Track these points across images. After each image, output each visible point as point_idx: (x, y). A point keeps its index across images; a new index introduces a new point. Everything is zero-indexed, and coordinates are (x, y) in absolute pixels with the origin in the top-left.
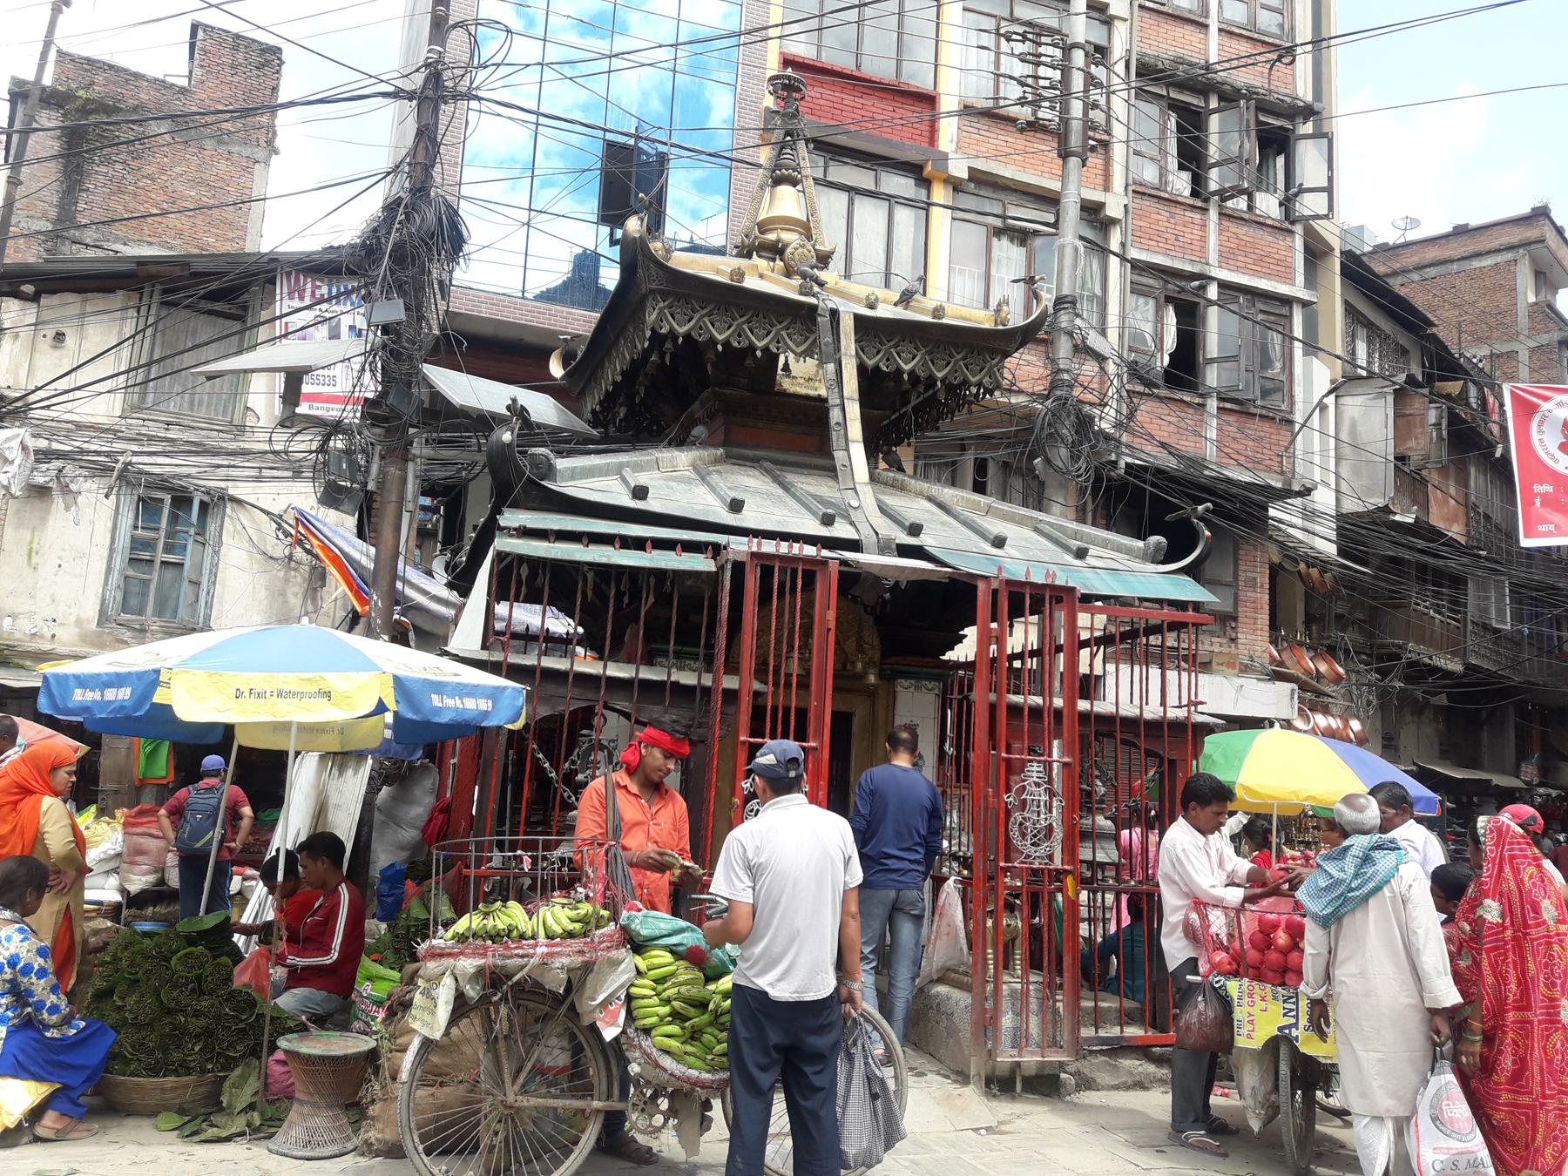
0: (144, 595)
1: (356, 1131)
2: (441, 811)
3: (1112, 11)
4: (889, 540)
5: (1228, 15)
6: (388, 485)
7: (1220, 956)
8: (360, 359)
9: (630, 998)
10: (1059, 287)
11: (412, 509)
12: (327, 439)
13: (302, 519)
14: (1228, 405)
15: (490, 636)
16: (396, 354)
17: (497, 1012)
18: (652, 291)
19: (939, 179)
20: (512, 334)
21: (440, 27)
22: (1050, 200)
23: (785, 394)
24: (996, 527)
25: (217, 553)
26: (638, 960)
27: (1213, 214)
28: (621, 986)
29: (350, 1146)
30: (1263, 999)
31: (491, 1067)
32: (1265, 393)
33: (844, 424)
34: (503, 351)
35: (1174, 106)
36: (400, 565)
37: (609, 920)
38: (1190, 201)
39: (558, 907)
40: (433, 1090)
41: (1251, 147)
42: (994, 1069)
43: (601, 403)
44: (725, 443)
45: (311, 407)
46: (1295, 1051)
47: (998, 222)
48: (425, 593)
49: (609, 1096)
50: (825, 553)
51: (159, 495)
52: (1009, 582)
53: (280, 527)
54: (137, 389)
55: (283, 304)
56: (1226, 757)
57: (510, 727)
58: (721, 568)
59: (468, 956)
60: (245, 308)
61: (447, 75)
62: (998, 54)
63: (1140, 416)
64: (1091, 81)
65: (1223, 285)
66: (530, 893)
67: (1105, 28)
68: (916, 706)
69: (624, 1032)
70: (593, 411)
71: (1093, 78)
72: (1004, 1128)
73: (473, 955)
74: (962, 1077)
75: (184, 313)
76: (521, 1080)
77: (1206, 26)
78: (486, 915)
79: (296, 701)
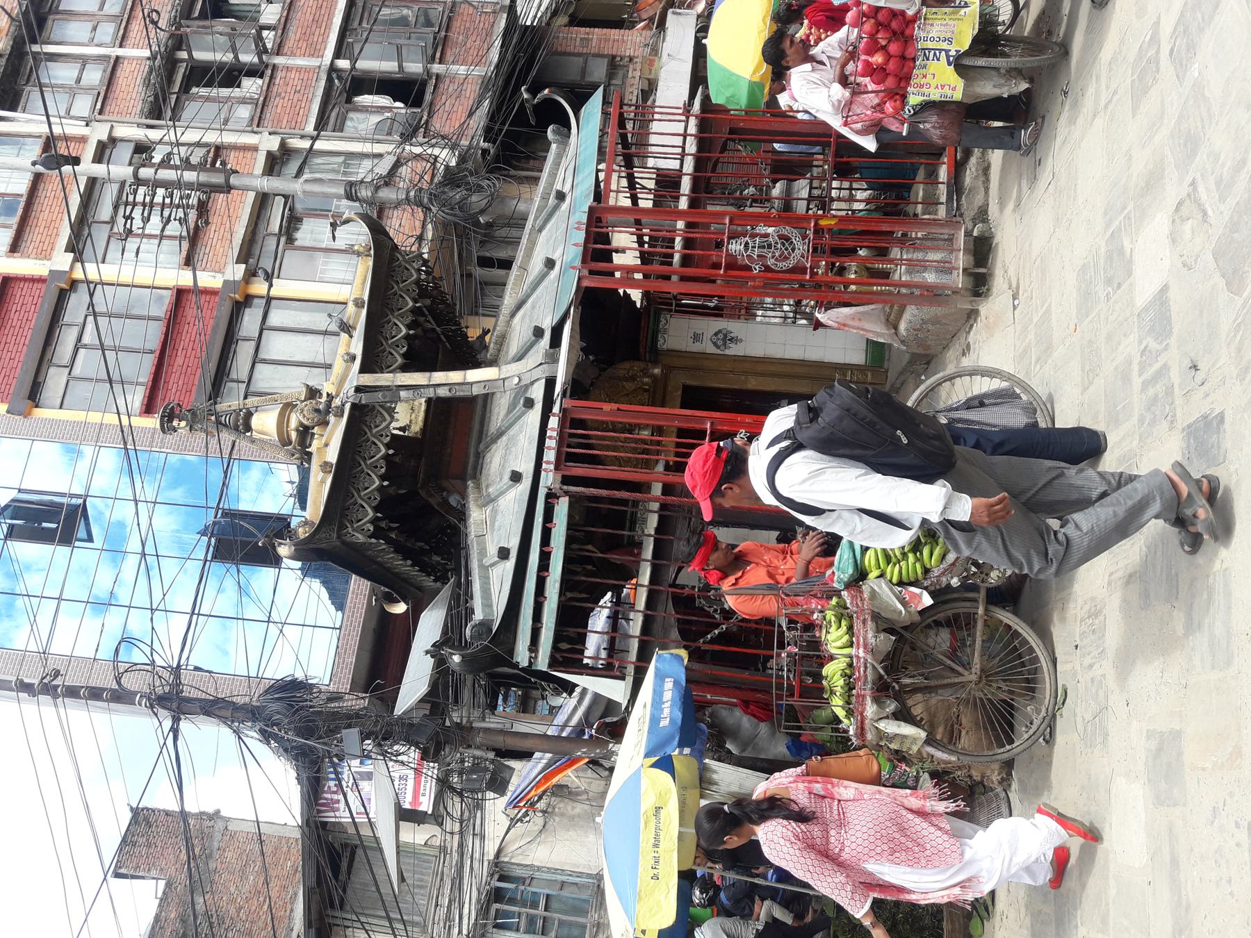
0: (570, 924)
1: (992, 790)
2: (747, 707)
3: (104, 137)
4: (547, 354)
5: (108, 39)
6: (490, 743)
7: (889, 107)
8: (391, 764)
9: (901, 583)
10: (339, 197)
11: (505, 718)
12: (453, 790)
13: (514, 804)
14: (438, 55)
15: (610, 670)
16: (385, 732)
17: (907, 685)
18: (339, 537)
19: (246, 288)
20: (370, 637)
21: (120, 696)
22: (263, 201)
23: (424, 429)
24: (537, 265)
25: (539, 869)
26: (872, 575)
27: (279, 60)
28: (891, 590)
29: (1003, 795)
30: (925, 76)
31: (950, 691)
32: (429, 23)
33: (450, 385)
34: (382, 652)
35: (185, 88)
36: (551, 731)
37: (840, 596)
38: (267, 79)
39: (829, 637)
40: (963, 733)
41: (222, 25)
42: (967, 289)
43: (429, 575)
44: (463, 478)
45: (424, 795)
46: (967, 54)
47: (283, 239)
48: (575, 709)
49: (975, 600)
50: (556, 409)
51: (493, 912)
52: (584, 261)
53: (520, 820)
54: (409, 928)
55: (343, 816)
56: (729, 86)
57: (686, 661)
58: (566, 493)
59: (864, 710)
60: (346, 845)
61: (159, 691)
62: (143, 236)
63: (447, 130)
64: (165, 163)
65: (338, 54)
66: (815, 655)
67: (119, 144)
68: (680, 334)
69: (926, 588)
70: (435, 581)
71: (163, 161)
72: (1014, 285)
73: (863, 705)
74: (972, 315)
75: (349, 891)
76: (960, 669)
77: (118, 58)
78: (832, 693)
79: (662, 835)
